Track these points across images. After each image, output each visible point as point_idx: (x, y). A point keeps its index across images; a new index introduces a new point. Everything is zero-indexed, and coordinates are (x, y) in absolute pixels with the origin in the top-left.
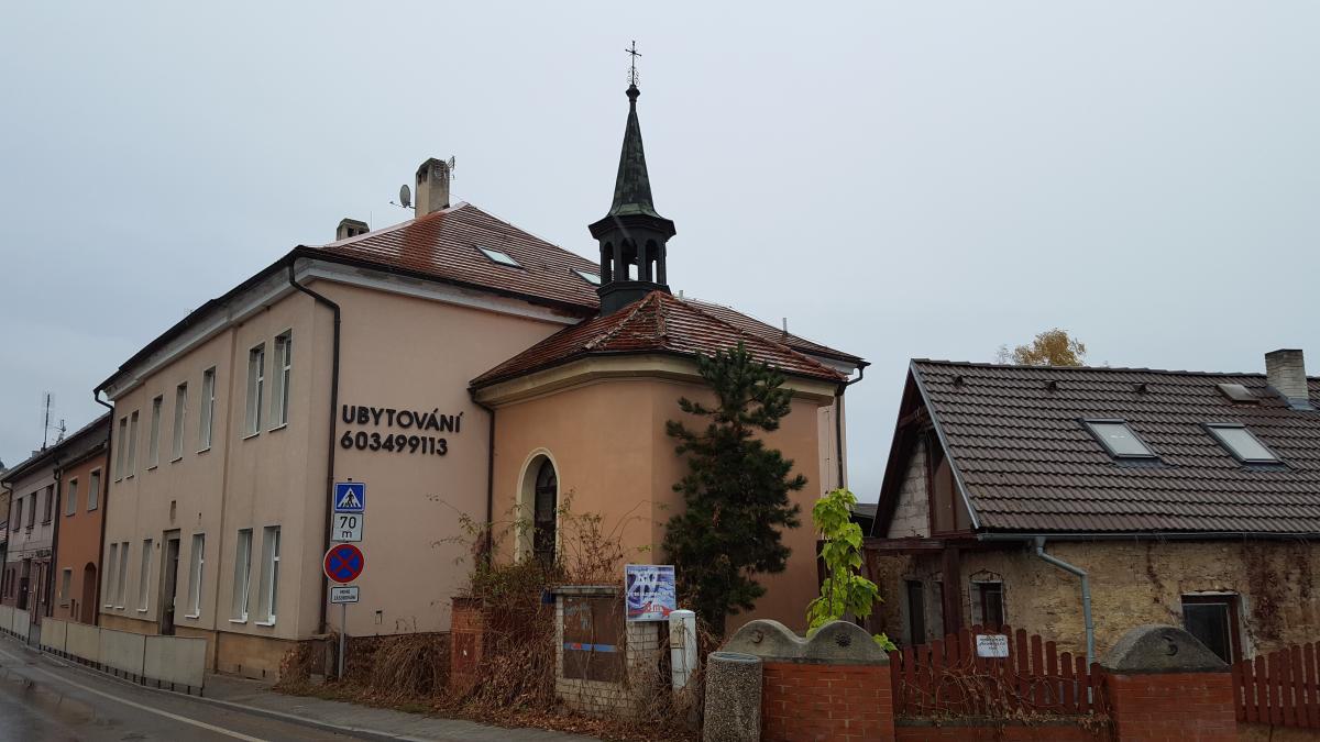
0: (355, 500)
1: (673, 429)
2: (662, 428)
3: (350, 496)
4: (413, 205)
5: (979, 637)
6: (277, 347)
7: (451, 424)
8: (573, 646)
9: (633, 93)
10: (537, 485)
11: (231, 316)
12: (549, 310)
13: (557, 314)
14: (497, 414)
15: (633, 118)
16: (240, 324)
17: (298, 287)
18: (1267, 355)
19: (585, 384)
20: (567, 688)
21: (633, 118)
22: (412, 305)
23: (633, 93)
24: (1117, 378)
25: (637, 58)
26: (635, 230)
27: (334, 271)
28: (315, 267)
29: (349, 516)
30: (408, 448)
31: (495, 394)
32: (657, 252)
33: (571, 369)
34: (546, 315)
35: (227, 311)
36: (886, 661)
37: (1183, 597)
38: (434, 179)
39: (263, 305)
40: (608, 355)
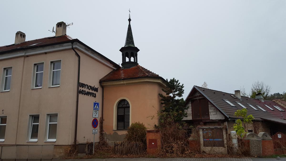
0: (97, 107)
1: (160, 95)
2: (158, 94)
3: (96, 106)
4: (55, 32)
5: (278, 134)
6: (50, 64)
7: (96, 90)
8: (205, 140)
9: (130, 20)
10: (118, 106)
11: (25, 53)
12: (112, 65)
13: (113, 67)
14: (104, 89)
15: (130, 25)
16: (27, 56)
17: (73, 49)
18: (235, 91)
19: (128, 85)
20: (203, 148)
21: (130, 25)
22: (36, 57)
23: (130, 20)
24: (218, 92)
25: (130, 13)
26: (130, 50)
27: (80, 47)
28: (77, 45)
29: (96, 111)
30: (90, 95)
31: (104, 84)
32: (135, 56)
33: (139, 80)
34: (111, 66)
35: (25, 52)
36: (271, 139)
37: (249, 131)
38: (64, 27)
39: (45, 52)
40: (151, 77)
